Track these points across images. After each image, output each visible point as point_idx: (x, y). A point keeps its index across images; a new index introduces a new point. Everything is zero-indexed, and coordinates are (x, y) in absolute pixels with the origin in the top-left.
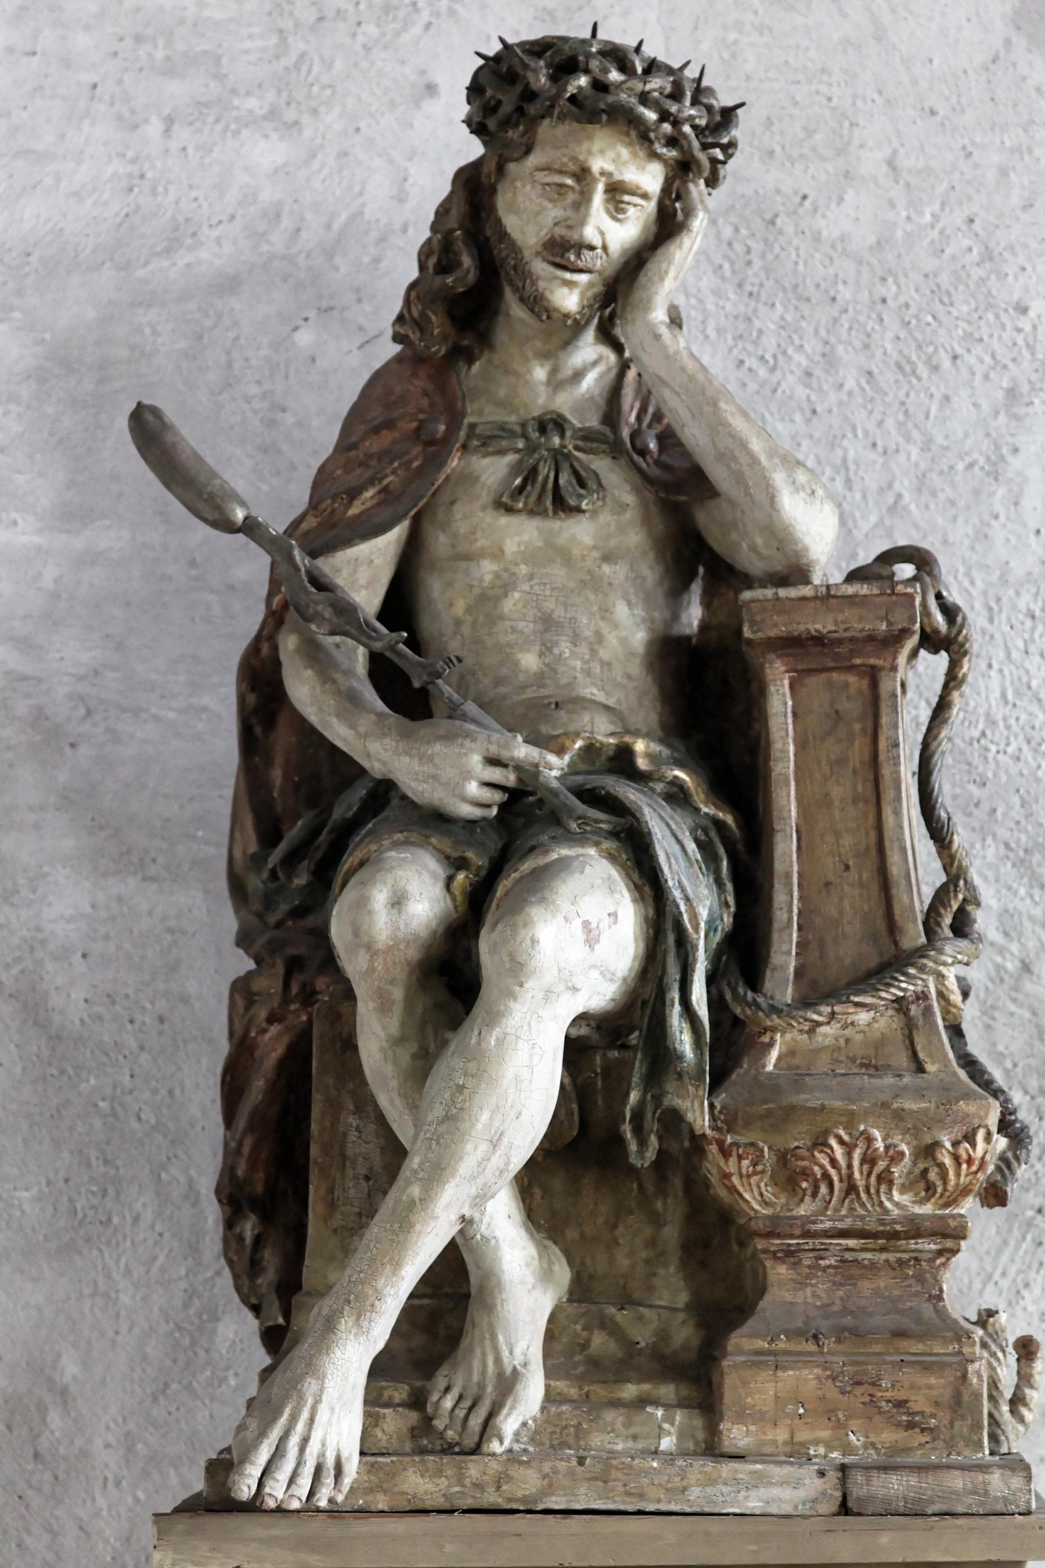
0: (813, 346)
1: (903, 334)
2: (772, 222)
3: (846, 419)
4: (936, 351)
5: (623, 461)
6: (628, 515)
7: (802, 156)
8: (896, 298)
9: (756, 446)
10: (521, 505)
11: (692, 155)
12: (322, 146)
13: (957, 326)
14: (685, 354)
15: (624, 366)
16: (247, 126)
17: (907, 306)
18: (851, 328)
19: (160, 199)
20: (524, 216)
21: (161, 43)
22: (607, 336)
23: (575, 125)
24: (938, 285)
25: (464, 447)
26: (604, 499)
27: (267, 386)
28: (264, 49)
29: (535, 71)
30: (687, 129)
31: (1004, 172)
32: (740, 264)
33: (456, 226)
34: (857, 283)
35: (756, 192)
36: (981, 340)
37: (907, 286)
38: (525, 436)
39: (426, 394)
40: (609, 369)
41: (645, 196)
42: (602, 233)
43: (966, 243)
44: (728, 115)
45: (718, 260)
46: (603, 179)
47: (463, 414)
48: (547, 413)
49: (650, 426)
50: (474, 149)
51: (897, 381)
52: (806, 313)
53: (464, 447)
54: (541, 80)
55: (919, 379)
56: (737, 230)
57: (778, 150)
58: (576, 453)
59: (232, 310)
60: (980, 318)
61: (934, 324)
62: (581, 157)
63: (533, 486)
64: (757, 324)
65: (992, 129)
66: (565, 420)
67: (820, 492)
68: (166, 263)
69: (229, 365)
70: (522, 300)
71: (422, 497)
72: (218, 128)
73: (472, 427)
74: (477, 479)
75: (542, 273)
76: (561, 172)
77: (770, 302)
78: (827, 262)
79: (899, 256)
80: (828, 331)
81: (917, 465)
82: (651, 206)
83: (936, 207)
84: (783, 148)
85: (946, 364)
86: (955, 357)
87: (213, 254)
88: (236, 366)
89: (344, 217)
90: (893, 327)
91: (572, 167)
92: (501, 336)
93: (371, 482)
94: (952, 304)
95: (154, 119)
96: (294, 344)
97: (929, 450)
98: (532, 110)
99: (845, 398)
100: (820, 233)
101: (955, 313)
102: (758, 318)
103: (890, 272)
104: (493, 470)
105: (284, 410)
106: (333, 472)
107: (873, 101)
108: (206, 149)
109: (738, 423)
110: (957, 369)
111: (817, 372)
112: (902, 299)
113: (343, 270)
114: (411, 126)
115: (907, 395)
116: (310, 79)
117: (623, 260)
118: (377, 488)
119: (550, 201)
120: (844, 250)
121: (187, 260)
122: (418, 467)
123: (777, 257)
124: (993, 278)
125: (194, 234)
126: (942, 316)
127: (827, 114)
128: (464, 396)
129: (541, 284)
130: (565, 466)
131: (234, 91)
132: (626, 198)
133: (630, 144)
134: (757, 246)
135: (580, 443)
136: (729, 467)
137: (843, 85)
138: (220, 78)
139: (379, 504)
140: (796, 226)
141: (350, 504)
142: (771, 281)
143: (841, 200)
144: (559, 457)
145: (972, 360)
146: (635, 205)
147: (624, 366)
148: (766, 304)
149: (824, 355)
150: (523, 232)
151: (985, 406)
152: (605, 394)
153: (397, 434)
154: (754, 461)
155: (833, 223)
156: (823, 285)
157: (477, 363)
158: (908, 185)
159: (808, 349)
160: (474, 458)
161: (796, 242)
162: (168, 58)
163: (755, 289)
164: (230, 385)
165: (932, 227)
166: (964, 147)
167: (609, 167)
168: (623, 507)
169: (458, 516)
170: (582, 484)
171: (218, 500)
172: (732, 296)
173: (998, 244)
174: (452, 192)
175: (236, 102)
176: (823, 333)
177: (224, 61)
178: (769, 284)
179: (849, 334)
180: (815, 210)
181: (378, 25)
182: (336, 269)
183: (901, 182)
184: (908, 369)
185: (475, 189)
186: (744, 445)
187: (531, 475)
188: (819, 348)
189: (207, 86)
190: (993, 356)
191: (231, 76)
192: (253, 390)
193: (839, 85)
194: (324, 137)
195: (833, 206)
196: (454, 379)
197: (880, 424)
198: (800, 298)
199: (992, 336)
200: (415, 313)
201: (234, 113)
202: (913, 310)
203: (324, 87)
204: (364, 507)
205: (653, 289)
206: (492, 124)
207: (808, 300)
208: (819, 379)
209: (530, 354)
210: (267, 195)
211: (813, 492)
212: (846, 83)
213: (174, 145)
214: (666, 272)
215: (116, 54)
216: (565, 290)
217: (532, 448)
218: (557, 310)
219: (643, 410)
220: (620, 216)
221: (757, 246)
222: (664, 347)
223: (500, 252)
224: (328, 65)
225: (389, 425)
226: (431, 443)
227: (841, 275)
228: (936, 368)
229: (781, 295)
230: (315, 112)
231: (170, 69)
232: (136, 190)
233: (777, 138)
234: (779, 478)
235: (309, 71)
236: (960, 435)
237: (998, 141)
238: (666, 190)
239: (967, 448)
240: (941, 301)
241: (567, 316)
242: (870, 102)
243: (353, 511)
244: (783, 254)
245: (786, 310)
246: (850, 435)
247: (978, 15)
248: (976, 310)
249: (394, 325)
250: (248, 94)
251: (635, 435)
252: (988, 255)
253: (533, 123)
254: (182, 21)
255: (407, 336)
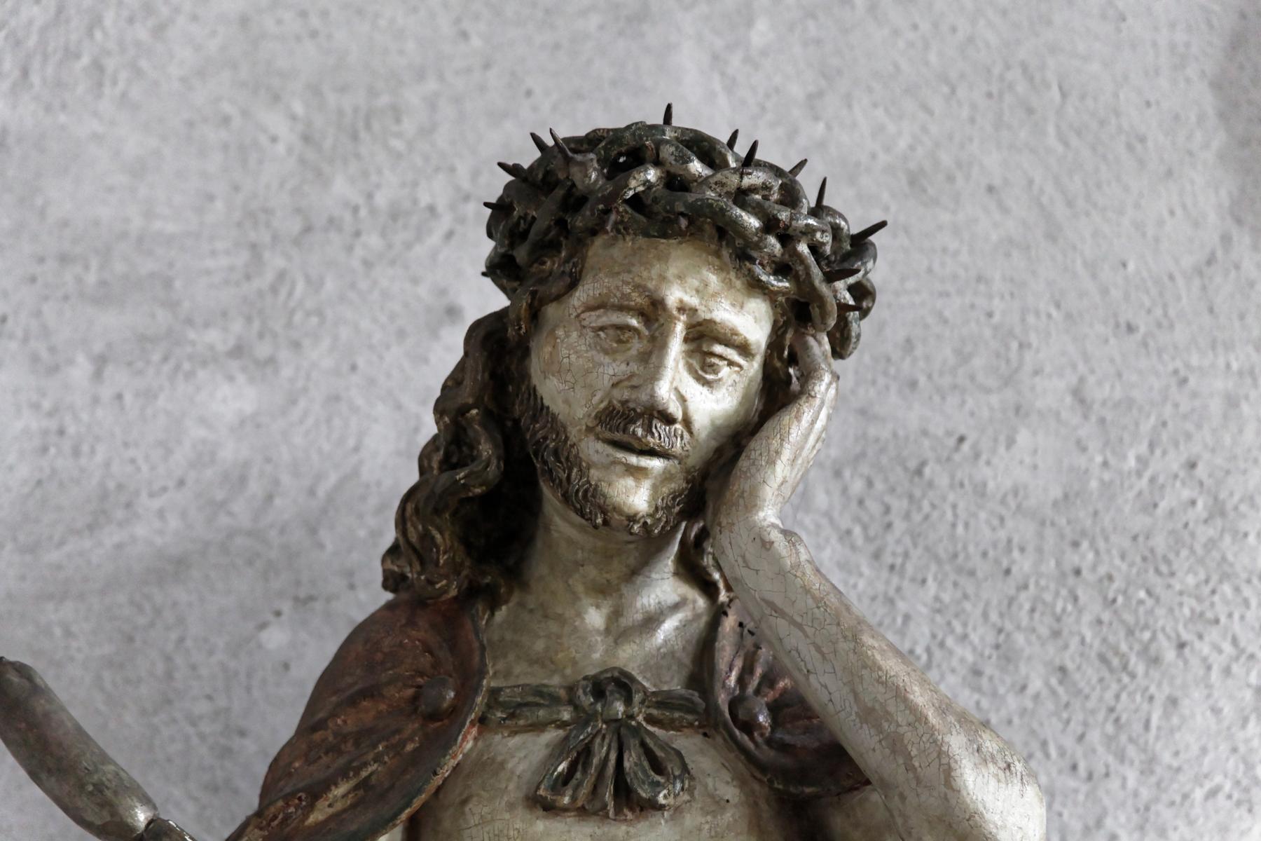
0: (981, 635)
1: (1106, 616)
2: (919, 472)
3: (1033, 732)
4: (1153, 638)
5: (719, 739)
6: (728, 816)
7: (955, 387)
8: (1094, 568)
9: (919, 697)
10: (566, 800)
11: (813, 288)
12: (305, 390)
13: (1181, 605)
14: (808, 570)
15: (718, 612)
16: (204, 364)
17: (1110, 578)
18: (1033, 610)
19: (83, 461)
20: (569, 377)
21: (94, 264)
22: (692, 570)
23: (641, 240)
24: (1152, 551)
25: (482, 721)
26: (691, 791)
27: (222, 702)
28: (232, 269)
29: (583, 165)
30: (803, 248)
31: (1232, 402)
32: (874, 529)
33: (470, 401)
34: (1039, 550)
35: (895, 435)
36: (1217, 621)
37: (1109, 551)
38: (572, 702)
39: (428, 649)
40: (697, 617)
41: (744, 349)
42: (683, 400)
43: (1186, 494)
44: (860, 244)
45: (845, 523)
46: (683, 318)
47: (482, 673)
48: (606, 671)
49: (757, 692)
50: (495, 300)
51: (1101, 680)
52: (970, 590)
53: (482, 721)
54: (593, 175)
55: (1133, 676)
56: (870, 484)
57: (922, 380)
58: (650, 728)
59: (175, 604)
60: (1213, 592)
61: (1150, 602)
62: (651, 285)
63: (585, 772)
64: (902, 606)
65: (1214, 348)
66: (632, 679)
67: (1018, 767)
68: (87, 543)
69: (169, 676)
70: (566, 499)
71: (419, 791)
72: (166, 368)
73: (494, 692)
74: (502, 765)
75: (595, 458)
76: (621, 308)
77: (920, 577)
78: (996, 522)
79: (1096, 513)
80: (1001, 615)
81: (1136, 794)
82: (753, 368)
83: (1143, 448)
84: (930, 377)
85: (1170, 655)
86: (1181, 646)
87: (153, 529)
88: (177, 675)
89: (333, 478)
90: (1094, 608)
91: (638, 300)
92: (539, 568)
93: (344, 774)
94: (1172, 574)
95: (81, 359)
96: (260, 646)
97: (1152, 772)
98: (579, 222)
99: (1029, 704)
100: (985, 485)
101: (1178, 587)
102: (903, 598)
103: (1083, 533)
104: (526, 753)
105: (242, 733)
106: (291, 763)
107: (1049, 316)
108: (149, 395)
109: (891, 665)
110: (1186, 662)
111: (989, 670)
112: (1102, 570)
113: (330, 547)
114: (426, 361)
115: (1117, 697)
116: (292, 304)
117: (714, 444)
118: (352, 783)
119: (606, 352)
120: (1019, 507)
121: (116, 538)
122: (415, 750)
123: (927, 517)
124: (1228, 539)
125: (128, 505)
126: (1158, 590)
127: (988, 333)
128: (483, 648)
129: (594, 474)
130: (633, 743)
131: (189, 322)
132: (718, 349)
133: (721, 269)
134: (899, 505)
135: (655, 712)
136: (880, 730)
137: (1007, 297)
138: (172, 305)
139: (353, 806)
140: (952, 477)
141: (311, 807)
142: (919, 551)
143: (1011, 442)
144: (622, 731)
145: (1205, 649)
146: (731, 363)
147: (718, 612)
148: (913, 580)
149: (997, 647)
150: (567, 402)
151: (1228, 709)
152: (690, 649)
153: (383, 707)
154: (918, 718)
155: (1002, 471)
156: (991, 553)
157: (504, 608)
158: (1102, 421)
159: (974, 638)
160: (498, 737)
161: (951, 497)
162: (103, 283)
163: (899, 561)
164: (169, 702)
165: (1139, 474)
166: (1176, 372)
167: (693, 300)
168: (720, 804)
169: (473, 820)
170: (657, 767)
171: (109, 793)
172: (866, 570)
173: (1231, 494)
174: (466, 354)
175: (192, 335)
176: (994, 617)
177: (178, 284)
178: (916, 554)
179: (1031, 618)
180: (977, 456)
181: (383, 234)
182: (321, 546)
183: (1093, 419)
184: (1116, 662)
185: (498, 352)
186: (900, 695)
187: (583, 756)
188: (991, 638)
189: (153, 316)
190: (1235, 641)
191: (186, 304)
192: (203, 707)
193: (1002, 297)
194: (308, 377)
195: (1001, 449)
196: (469, 625)
197: (1081, 738)
198: (959, 570)
199: (1230, 615)
200: (414, 537)
201: (189, 349)
202: (1118, 584)
203: (308, 314)
204: (331, 811)
205: (759, 478)
206: (521, 254)
207: (972, 573)
208: (991, 678)
209: (580, 588)
210: (229, 452)
211: (1009, 766)
212: (1012, 294)
213: (106, 392)
214: (778, 453)
215: (33, 280)
216: (630, 482)
217: (584, 718)
218: (617, 509)
219: (747, 670)
220: (709, 377)
221: (899, 505)
222: (777, 560)
223: (535, 433)
224: (315, 284)
225: (370, 693)
226: (434, 716)
227: (1016, 540)
228: (1155, 661)
229: (933, 567)
230: (296, 345)
231: (104, 296)
232: (53, 450)
233: (921, 364)
234: (956, 743)
235: (290, 294)
236: (1195, 750)
237: (1221, 362)
238: (775, 344)
239: (1205, 769)
240: (1157, 571)
241: (632, 518)
242: (1044, 318)
243: (316, 817)
244: (935, 515)
245: (941, 584)
246: (1039, 754)
247: (1184, 207)
248: (1207, 581)
249: (383, 561)
250: (207, 325)
251: (734, 704)
252: (1218, 510)
253: (581, 242)
254: (124, 235)
255: (403, 577)
